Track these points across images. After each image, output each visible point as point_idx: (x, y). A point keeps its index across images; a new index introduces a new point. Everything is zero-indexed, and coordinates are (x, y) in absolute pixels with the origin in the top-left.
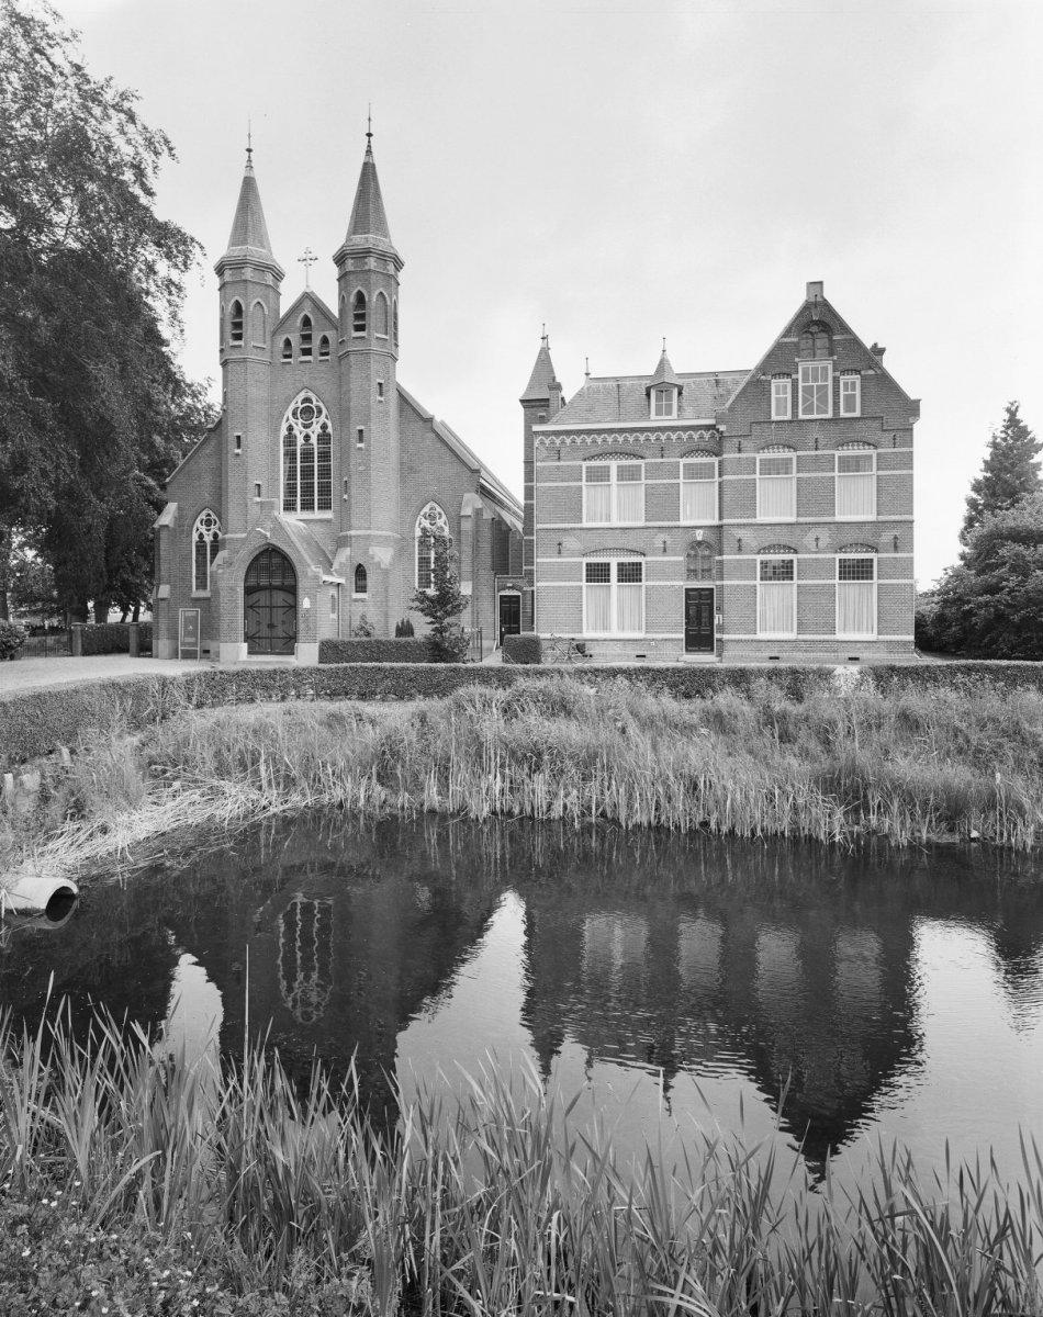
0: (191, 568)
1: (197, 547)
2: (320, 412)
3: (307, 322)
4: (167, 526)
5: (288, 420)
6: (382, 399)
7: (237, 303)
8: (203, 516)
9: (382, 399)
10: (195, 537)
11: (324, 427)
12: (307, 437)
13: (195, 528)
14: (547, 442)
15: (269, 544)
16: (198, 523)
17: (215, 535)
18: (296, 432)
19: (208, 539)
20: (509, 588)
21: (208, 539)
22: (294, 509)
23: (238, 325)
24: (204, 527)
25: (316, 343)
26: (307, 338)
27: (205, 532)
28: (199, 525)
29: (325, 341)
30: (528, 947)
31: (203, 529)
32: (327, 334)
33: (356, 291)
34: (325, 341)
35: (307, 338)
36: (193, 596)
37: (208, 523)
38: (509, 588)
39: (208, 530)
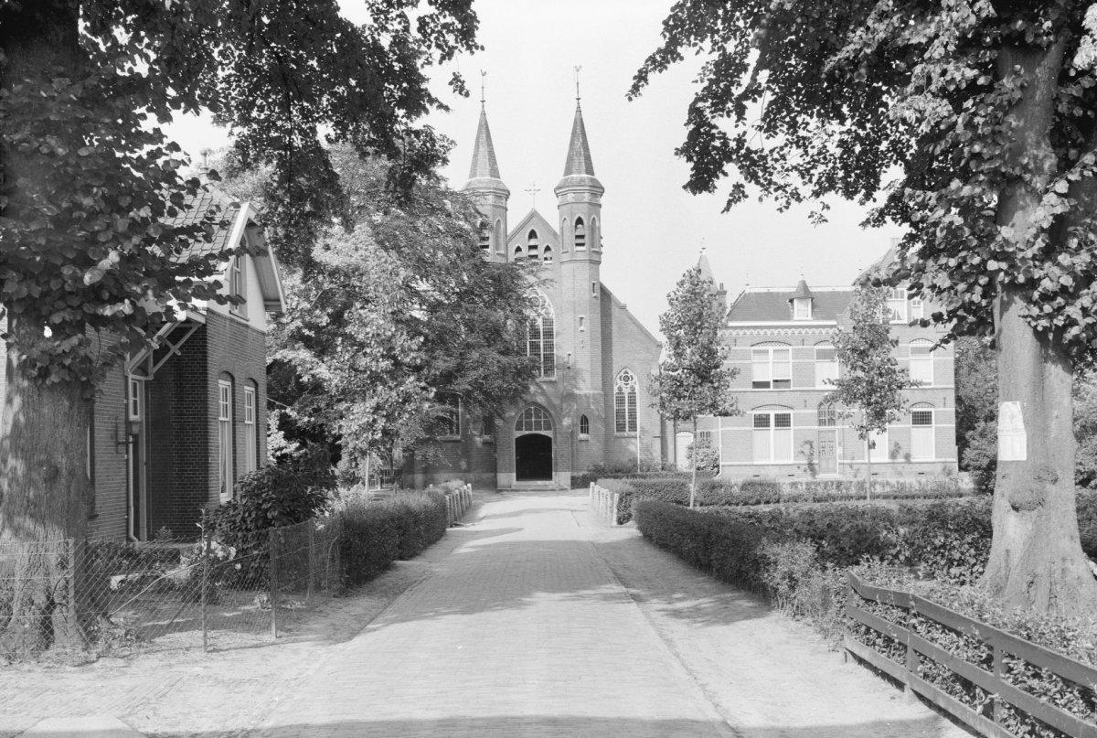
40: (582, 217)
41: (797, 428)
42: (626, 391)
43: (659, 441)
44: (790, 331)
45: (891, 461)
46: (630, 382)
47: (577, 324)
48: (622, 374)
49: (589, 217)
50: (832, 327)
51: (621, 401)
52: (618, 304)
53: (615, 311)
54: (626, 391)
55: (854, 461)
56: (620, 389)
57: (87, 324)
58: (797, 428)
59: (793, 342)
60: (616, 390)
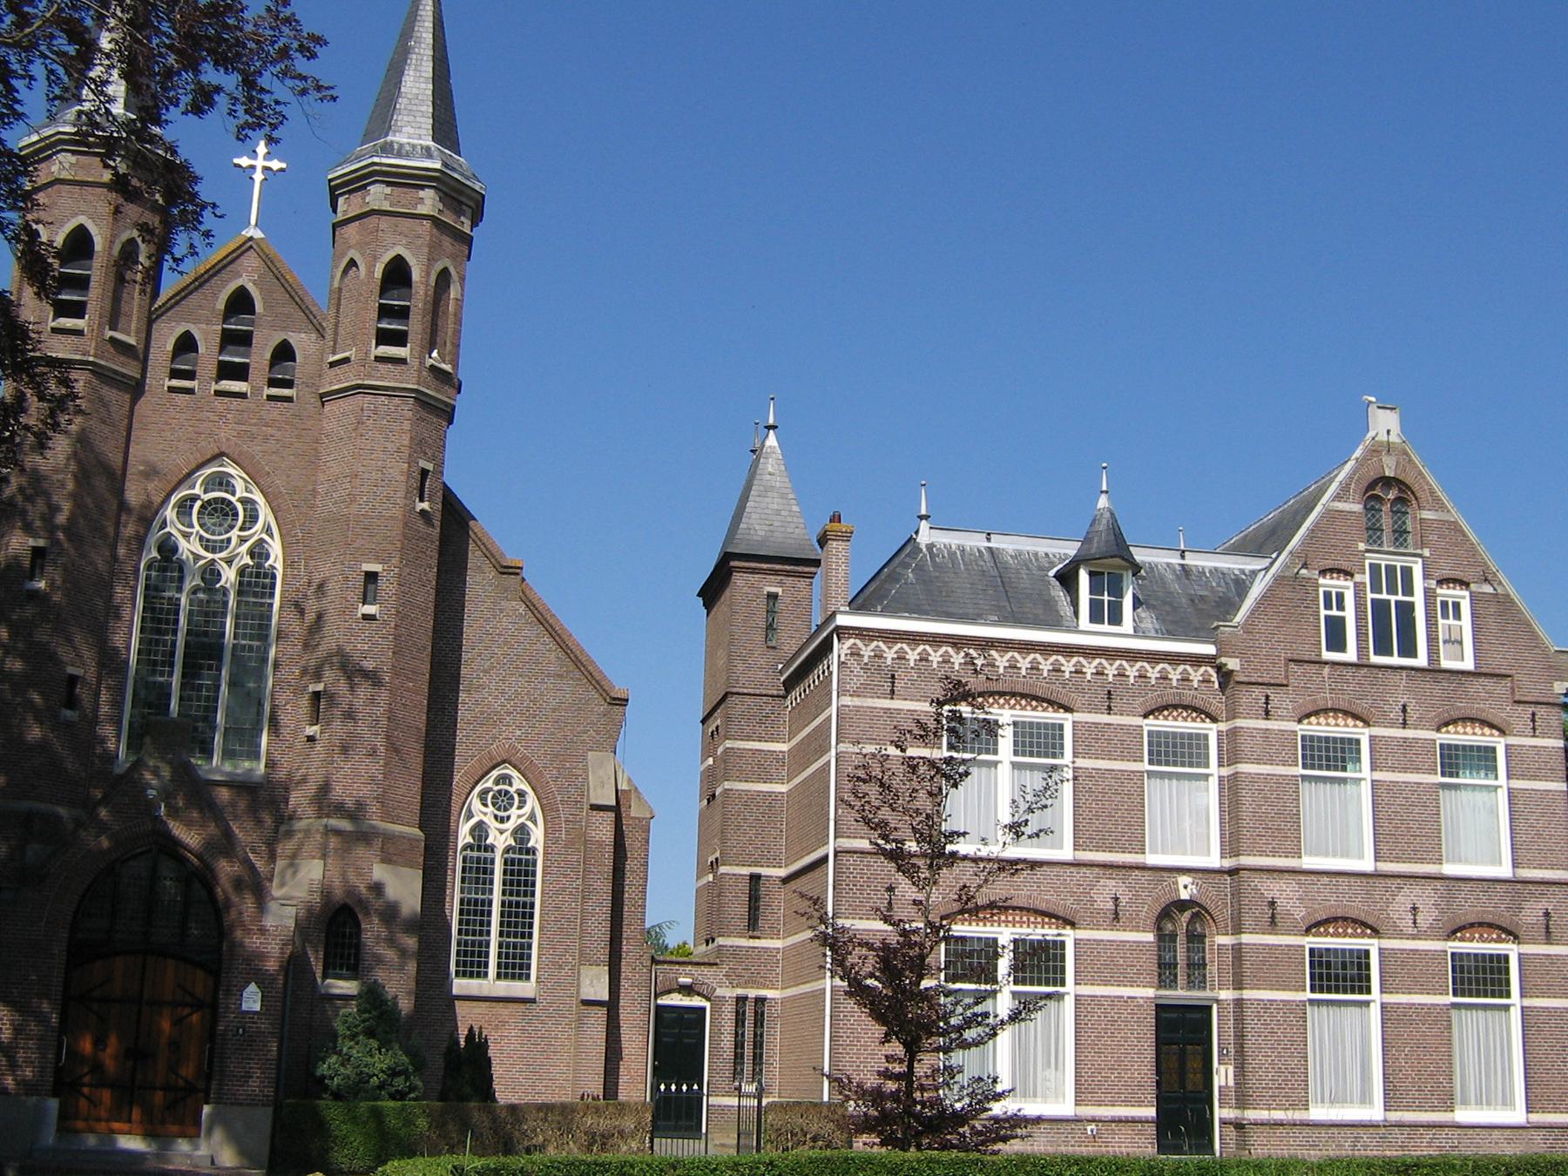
3: (240, 303)
14: (867, 652)
29: (284, 353)
33: (388, 256)
34: (284, 353)
35: (233, 340)
40: (251, 287)
41: (1086, 990)
42: (500, 840)
43: (599, 1017)
44: (1068, 666)
45: (1228, 863)
46: (514, 812)
47: (354, 595)
48: (488, 783)
49: (431, 260)
50: (1197, 660)
51: (479, 871)
52: (490, 555)
53: (479, 583)
54: (500, 840)
55: (1251, 1115)
56: (480, 830)
57: (263, 236)
58: (1086, 990)
59: (1076, 699)
60: (464, 835)
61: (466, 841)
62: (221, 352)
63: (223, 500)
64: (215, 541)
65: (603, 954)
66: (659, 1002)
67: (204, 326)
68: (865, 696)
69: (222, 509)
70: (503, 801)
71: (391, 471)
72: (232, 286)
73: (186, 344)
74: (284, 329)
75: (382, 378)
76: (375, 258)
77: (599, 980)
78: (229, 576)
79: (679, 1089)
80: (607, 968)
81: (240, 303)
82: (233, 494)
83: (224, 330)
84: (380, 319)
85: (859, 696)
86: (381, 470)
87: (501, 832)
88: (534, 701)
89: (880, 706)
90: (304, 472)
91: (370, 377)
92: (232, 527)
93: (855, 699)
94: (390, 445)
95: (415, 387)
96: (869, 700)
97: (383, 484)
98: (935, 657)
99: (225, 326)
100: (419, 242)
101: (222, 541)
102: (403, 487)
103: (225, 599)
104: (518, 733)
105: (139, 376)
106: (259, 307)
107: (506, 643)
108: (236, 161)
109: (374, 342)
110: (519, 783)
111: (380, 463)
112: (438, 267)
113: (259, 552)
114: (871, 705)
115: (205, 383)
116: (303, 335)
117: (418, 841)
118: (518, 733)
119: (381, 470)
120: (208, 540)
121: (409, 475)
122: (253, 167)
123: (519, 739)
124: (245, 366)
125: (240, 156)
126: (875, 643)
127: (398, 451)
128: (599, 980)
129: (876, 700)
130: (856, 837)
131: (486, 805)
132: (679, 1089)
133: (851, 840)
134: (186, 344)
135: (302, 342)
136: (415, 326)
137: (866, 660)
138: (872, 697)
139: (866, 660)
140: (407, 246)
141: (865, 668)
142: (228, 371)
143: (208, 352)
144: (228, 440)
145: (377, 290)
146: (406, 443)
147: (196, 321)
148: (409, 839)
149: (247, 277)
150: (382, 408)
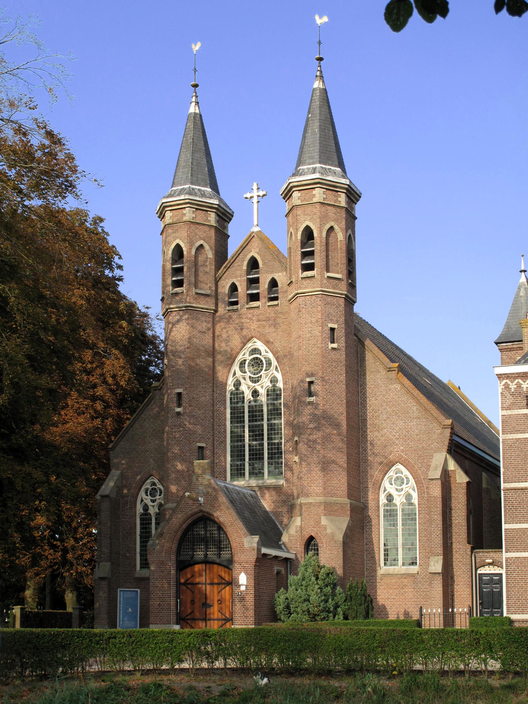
0: (135, 544)
1: (141, 519)
2: (269, 364)
3: (253, 264)
4: (107, 496)
5: (235, 374)
6: (335, 345)
7: (178, 247)
8: (147, 485)
9: (335, 345)
10: (139, 509)
11: (274, 380)
12: (255, 393)
13: (382, 489)
14: (513, 386)
15: (201, 511)
16: (142, 494)
17: (160, 506)
18: (243, 388)
19: (153, 511)
20: (490, 564)
21: (153, 511)
22: (243, 475)
23: (178, 271)
24: (149, 497)
25: (264, 285)
26: (254, 282)
27: (150, 504)
28: (144, 496)
29: (274, 283)
30: (367, 322)
31: (148, 500)
32: (277, 276)
33: (304, 226)
34: (274, 283)
35: (254, 282)
36: (137, 576)
37: (153, 493)
38: (490, 564)
39: (153, 501)
60: (383, 500)
61: (384, 502)
62: (248, 289)
63: (257, 358)
64: (255, 378)
65: (440, 550)
66: (479, 572)
67: (239, 279)
68: (513, 409)
69: (257, 362)
70: (400, 481)
71: (315, 332)
72: (249, 257)
73: (234, 288)
74: (272, 272)
75: (306, 288)
76: (297, 230)
77: (438, 563)
78: (262, 392)
79: (432, 610)
80: (442, 557)
81: (253, 264)
82: (261, 354)
83: (248, 279)
84: (302, 260)
85: (510, 409)
86: (310, 332)
87: (153, 506)
88: (408, 432)
89: (521, 413)
90: (286, 339)
91: (300, 288)
92: (262, 370)
93: (508, 411)
94: (313, 320)
95: (320, 289)
96: (516, 411)
97: (312, 338)
98: (513, 386)
99: (248, 277)
100: (315, 217)
101: (258, 377)
102: (320, 339)
103: (243, 405)
104: (402, 448)
105: (214, 308)
106: (261, 265)
107: (393, 405)
108: (245, 196)
109: (300, 271)
110: (406, 472)
111: (309, 329)
112: (328, 226)
113: (274, 380)
114: (516, 413)
115: (243, 306)
116: (280, 274)
117: (346, 504)
118: (402, 448)
119: (310, 332)
120: (253, 378)
121: (322, 332)
122: (252, 197)
123: (402, 451)
124: (258, 294)
125: (246, 193)
126: (517, 380)
127: (317, 321)
128: (438, 563)
129: (519, 410)
130: (512, 482)
131: (147, 495)
132: (432, 610)
133: (509, 484)
134: (234, 288)
135: (281, 278)
136: (318, 260)
137: (513, 390)
138: (517, 409)
139: (513, 390)
140: (310, 220)
141: (513, 395)
142: (254, 297)
143: (242, 288)
144: (254, 330)
145: (299, 244)
146: (320, 317)
147: (236, 277)
148: (340, 504)
149: (254, 252)
150: (308, 302)
